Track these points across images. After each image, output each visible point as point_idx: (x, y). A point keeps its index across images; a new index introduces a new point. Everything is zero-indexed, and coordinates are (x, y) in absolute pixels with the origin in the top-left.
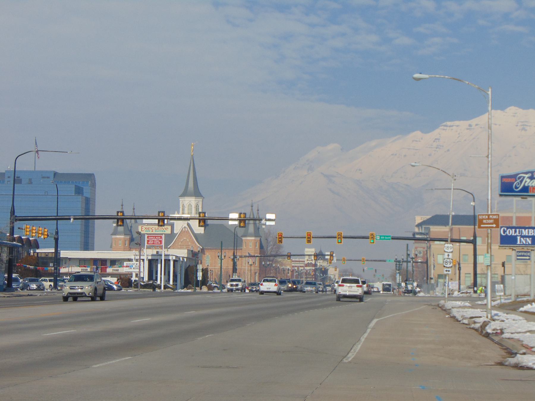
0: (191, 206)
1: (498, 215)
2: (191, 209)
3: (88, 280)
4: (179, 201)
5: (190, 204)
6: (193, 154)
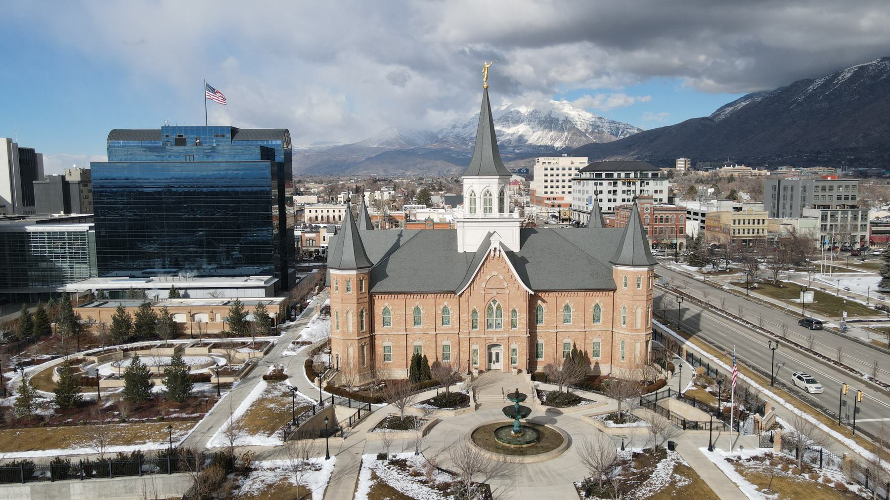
0: (490, 195)
1: (821, 451)
2: (490, 200)
3: (94, 473)
4: (33, 184)
5: (488, 192)
6: (487, 87)
